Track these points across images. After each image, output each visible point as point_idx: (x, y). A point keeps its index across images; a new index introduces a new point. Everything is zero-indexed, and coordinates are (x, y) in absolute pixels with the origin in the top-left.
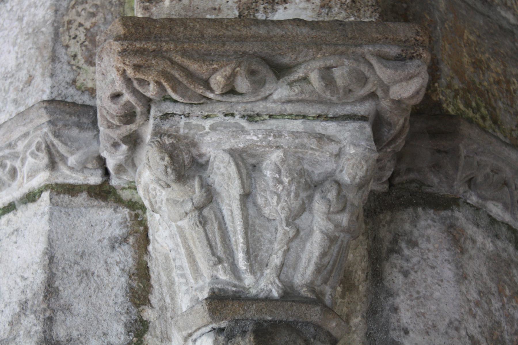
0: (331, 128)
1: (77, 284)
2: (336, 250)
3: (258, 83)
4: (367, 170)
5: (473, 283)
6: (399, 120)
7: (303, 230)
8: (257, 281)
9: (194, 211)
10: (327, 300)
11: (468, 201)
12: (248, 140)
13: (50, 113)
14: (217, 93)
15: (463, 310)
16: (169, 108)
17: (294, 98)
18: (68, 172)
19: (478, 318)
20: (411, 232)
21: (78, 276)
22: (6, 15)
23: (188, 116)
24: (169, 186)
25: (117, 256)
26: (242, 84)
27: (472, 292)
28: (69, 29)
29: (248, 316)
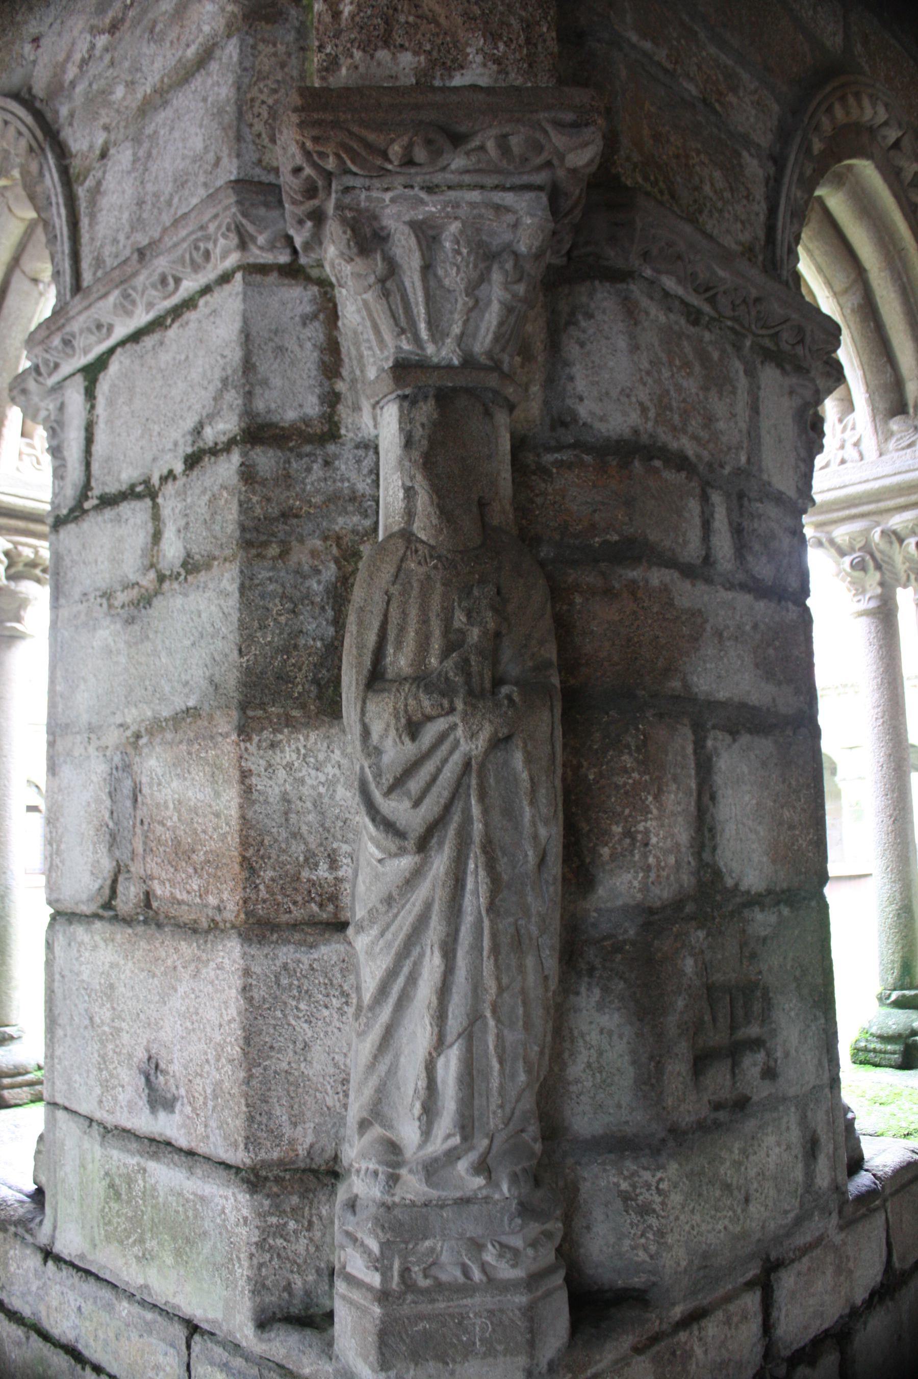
3: (436, 153)
4: (543, 241)
8: (439, 350)
10: (506, 367)
13: (237, 192)
16: (350, 181)
17: (471, 168)
18: (257, 252)
22: (191, 96)
23: (368, 189)
24: (352, 260)
25: (309, 332)
26: (420, 154)
28: (252, 107)
29: (430, 382)
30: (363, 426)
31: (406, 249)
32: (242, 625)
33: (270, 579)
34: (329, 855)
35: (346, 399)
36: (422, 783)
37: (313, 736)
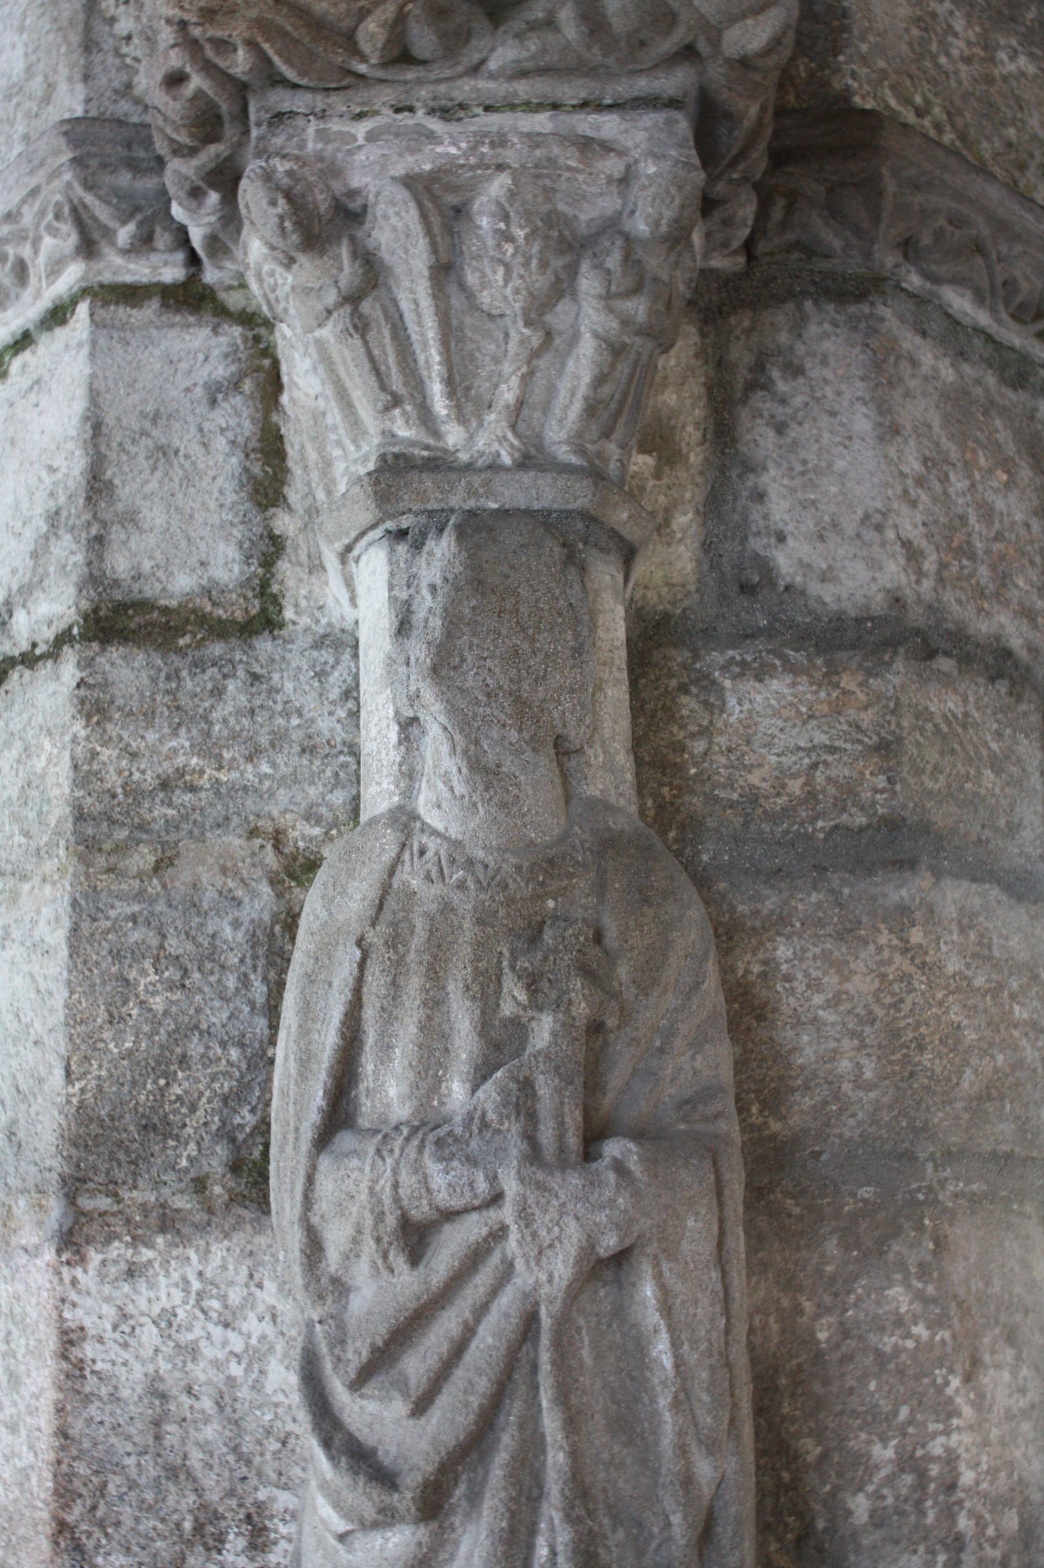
0: (608, 125)
1: (148, 472)
2: (627, 371)
3: (454, 41)
4: (682, 207)
5: (912, 442)
6: (748, 107)
7: (560, 334)
8: (471, 437)
9: (342, 305)
11: (904, 285)
12: (441, 155)
14: (374, 61)
15: (890, 492)
17: (529, 65)
19: (921, 507)
20: (791, 348)
21: (147, 458)
25: (220, 417)
27: (911, 459)
30: (330, 602)
31: (398, 233)
32: (74, 1018)
33: (134, 918)
34: (249, 1517)
35: (296, 548)
36: (433, 1361)
37: (218, 1251)
